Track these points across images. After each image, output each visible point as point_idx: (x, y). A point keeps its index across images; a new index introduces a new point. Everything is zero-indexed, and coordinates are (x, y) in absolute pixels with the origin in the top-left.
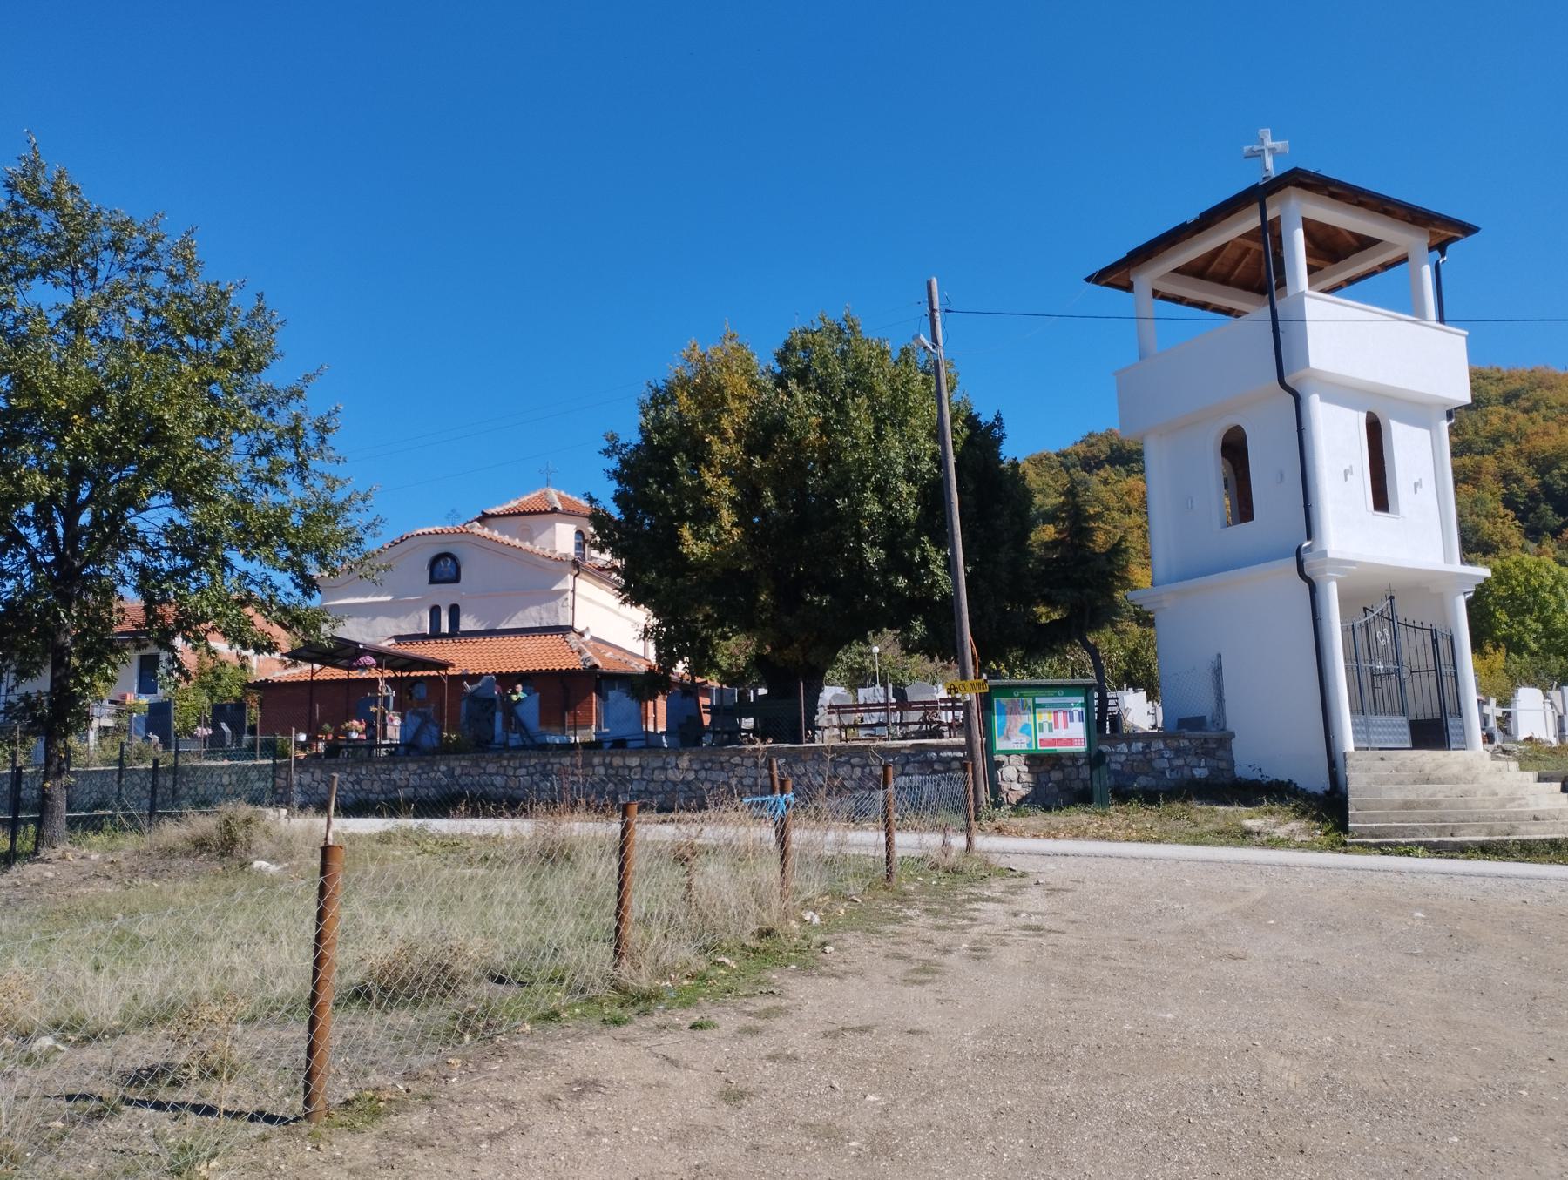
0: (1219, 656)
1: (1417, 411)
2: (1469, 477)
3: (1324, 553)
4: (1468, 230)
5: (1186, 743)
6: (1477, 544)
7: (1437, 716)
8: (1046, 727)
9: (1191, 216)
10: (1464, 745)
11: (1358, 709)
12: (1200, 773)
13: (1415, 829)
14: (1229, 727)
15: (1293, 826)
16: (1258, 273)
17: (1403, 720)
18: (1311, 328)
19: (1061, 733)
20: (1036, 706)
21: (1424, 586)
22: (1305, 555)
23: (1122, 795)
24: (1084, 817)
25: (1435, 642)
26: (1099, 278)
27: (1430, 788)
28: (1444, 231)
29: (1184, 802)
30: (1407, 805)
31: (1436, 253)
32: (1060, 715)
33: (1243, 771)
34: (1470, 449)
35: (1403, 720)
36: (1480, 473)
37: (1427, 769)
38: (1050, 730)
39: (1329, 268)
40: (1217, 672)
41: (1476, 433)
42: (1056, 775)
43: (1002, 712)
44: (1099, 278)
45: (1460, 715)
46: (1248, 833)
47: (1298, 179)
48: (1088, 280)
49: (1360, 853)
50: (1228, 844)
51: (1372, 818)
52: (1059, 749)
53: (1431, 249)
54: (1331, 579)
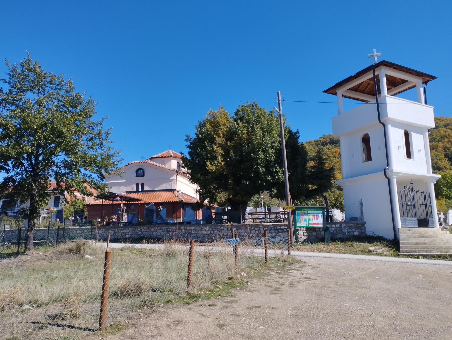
0: (362, 200)
1: (419, 130)
2: (434, 148)
3: (392, 170)
4: (434, 78)
5: (352, 225)
6: (437, 168)
7: (426, 218)
8: (311, 220)
9: (353, 74)
10: (433, 226)
11: (402, 215)
12: (356, 233)
13: (419, 251)
14: (365, 220)
15: (384, 250)
16: (373, 90)
17: (416, 219)
18: (388, 106)
19: (315, 221)
20: (308, 213)
21: (421, 180)
22: (386, 171)
23: (333, 240)
24: (322, 246)
25: (425, 196)
26: (327, 91)
27: (423, 239)
28: (427, 78)
29: (351, 242)
30: (417, 244)
31: (424, 84)
32: (315, 216)
33: (369, 233)
34: (434, 140)
35: (416, 219)
36: (437, 147)
37: (423, 233)
38: (313, 220)
39: (393, 89)
40: (361, 204)
41: (436, 136)
42: (314, 234)
43: (299, 215)
44: (327, 91)
45: (432, 218)
46: (370, 251)
47: (384, 64)
48: (324, 92)
49: (403, 257)
50: (364, 254)
51: (407, 247)
52: (315, 226)
53: (423, 83)
54: (394, 178)
